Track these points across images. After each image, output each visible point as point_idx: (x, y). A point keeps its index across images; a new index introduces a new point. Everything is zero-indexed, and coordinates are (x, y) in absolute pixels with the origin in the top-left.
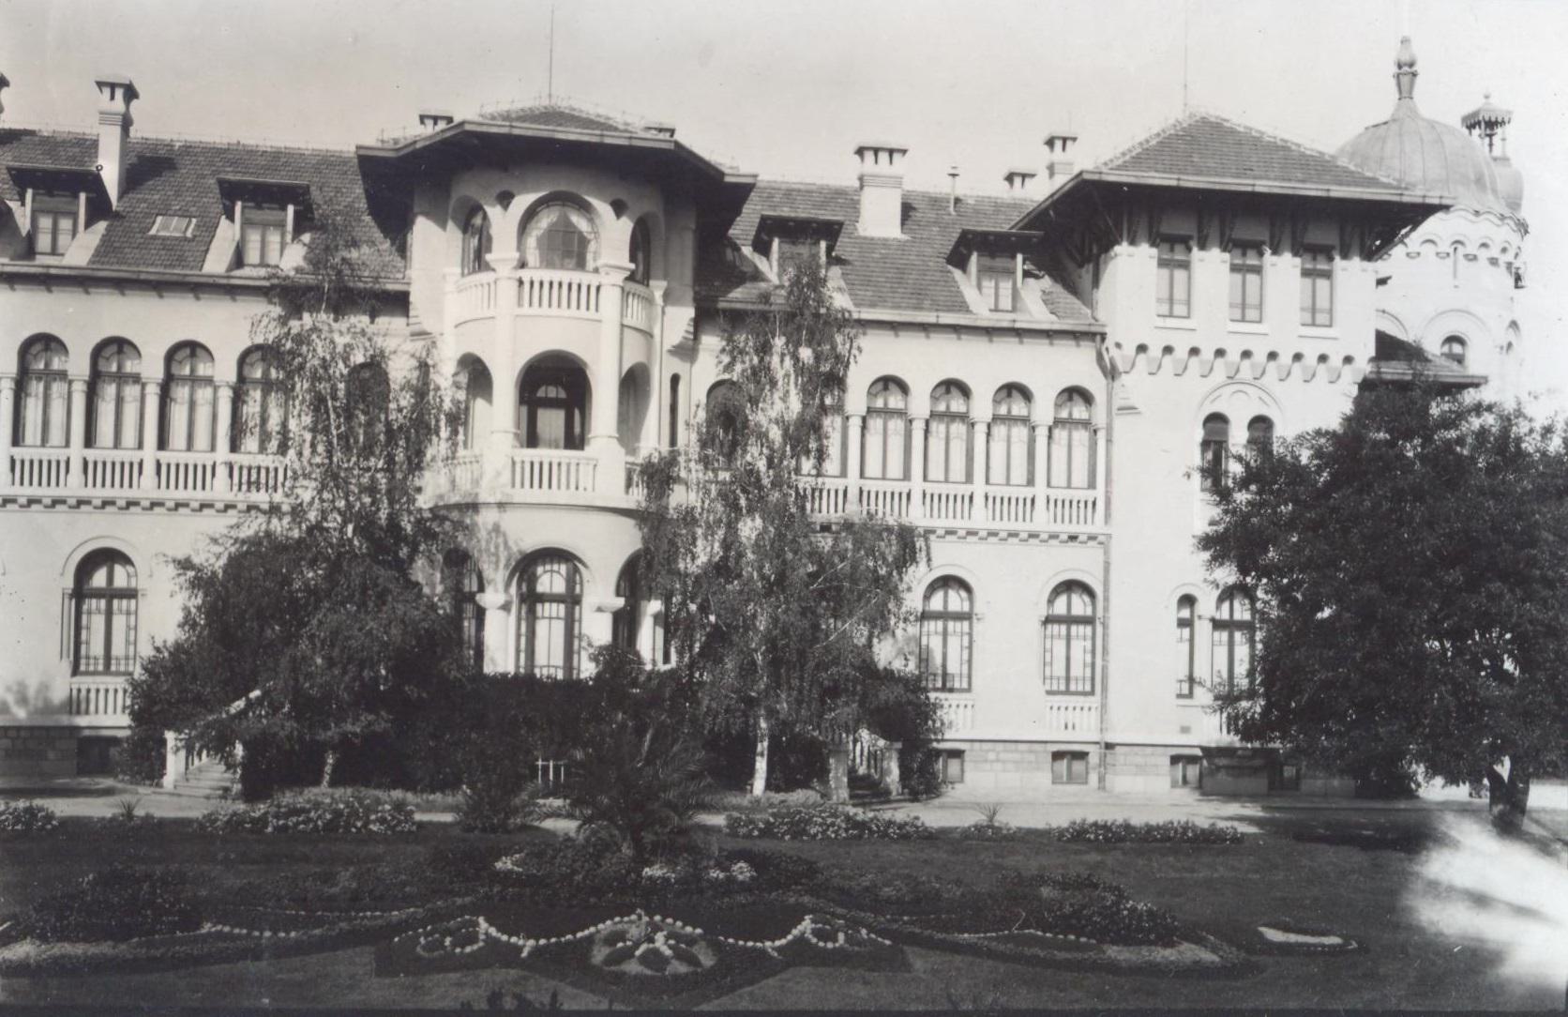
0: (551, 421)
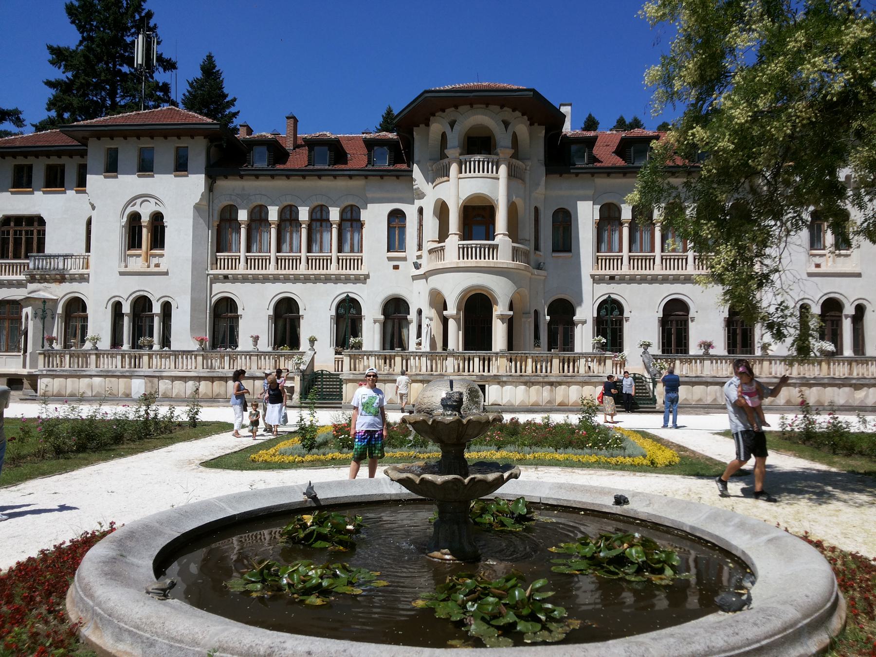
0: (480, 229)
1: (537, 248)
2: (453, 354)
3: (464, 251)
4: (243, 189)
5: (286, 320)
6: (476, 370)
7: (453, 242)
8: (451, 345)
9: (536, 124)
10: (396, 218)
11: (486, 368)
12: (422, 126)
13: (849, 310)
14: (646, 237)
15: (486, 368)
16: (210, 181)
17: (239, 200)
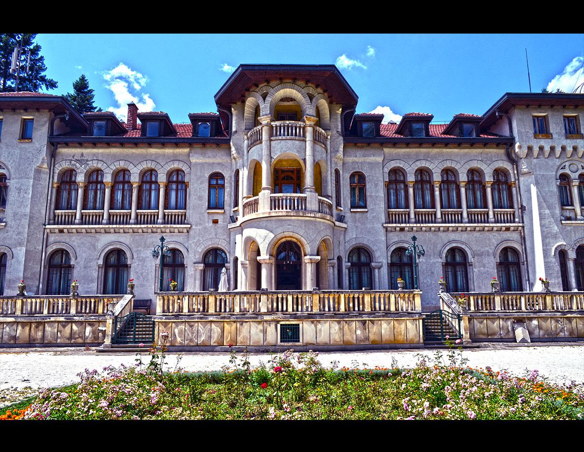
1: (338, 204)
2: (265, 292)
3: (275, 204)
4: (82, 155)
5: (116, 265)
6: (290, 309)
7: (265, 196)
8: (264, 285)
9: (334, 103)
10: (216, 181)
11: (34, 304)
12: (239, 103)
14: (232, 336)
15: (34, 304)
16: (53, 148)
17: (78, 164)
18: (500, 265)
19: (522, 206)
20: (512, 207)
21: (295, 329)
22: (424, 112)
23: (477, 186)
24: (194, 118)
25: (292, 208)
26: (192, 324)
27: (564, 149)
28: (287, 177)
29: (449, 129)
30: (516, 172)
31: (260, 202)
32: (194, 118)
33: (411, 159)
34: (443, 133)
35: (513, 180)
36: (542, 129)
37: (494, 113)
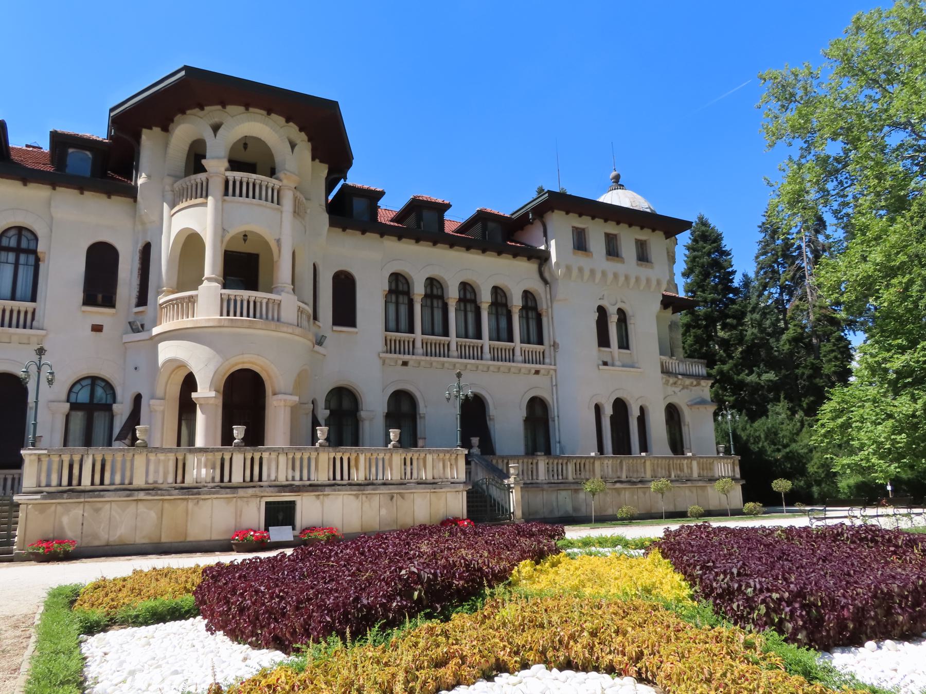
3: (228, 307)
13: (635, 413)
18: (527, 421)
19: (554, 342)
20: (540, 342)
21: (290, 507)
22: (438, 198)
23: (469, 307)
24: (60, 141)
25: (258, 314)
26: (99, 505)
27: (604, 274)
28: (243, 268)
29: (401, 217)
30: (549, 297)
31: (201, 301)
32: (60, 141)
33: (421, 261)
34: (391, 221)
35: (545, 307)
36: (580, 243)
37: (527, 214)
